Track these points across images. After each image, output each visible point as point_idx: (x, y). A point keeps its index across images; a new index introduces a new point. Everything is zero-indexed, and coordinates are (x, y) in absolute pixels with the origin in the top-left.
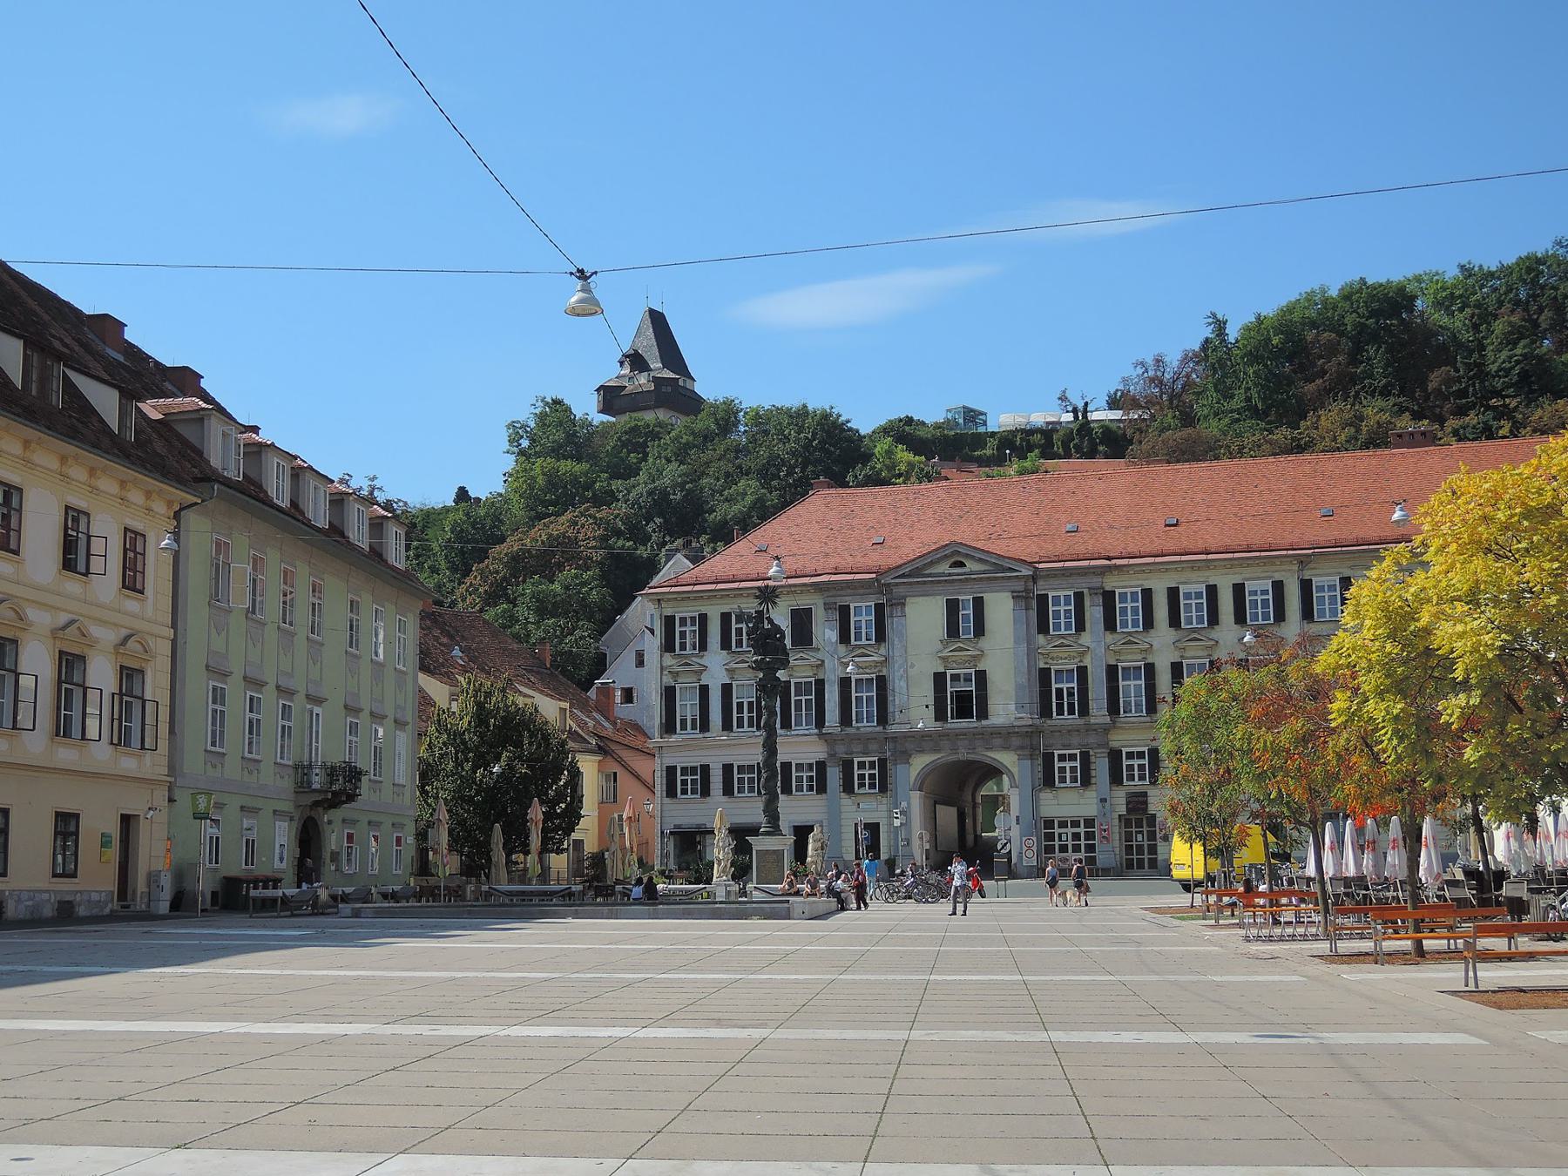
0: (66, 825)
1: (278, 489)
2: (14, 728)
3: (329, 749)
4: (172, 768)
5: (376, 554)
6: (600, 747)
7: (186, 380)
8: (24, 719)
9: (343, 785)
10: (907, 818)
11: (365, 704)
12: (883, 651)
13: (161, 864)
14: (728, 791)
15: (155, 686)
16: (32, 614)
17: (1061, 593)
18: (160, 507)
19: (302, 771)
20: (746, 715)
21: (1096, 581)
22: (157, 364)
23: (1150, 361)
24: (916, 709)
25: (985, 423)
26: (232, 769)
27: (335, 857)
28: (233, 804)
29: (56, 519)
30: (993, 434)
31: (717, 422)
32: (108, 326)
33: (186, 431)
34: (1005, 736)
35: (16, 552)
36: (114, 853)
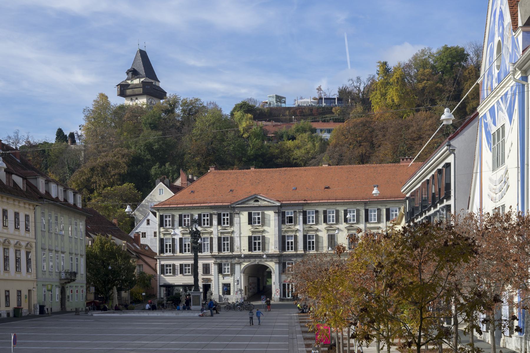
6: (137, 256)
11: (74, 252)
12: (232, 229)
13: (36, 302)
14: (181, 272)
17: (290, 211)
20: (187, 248)
21: (301, 208)
23: (355, 79)
24: (242, 246)
25: (285, 102)
27: (69, 297)
30: (289, 109)
31: (170, 105)
34: (270, 257)
36: (27, 300)
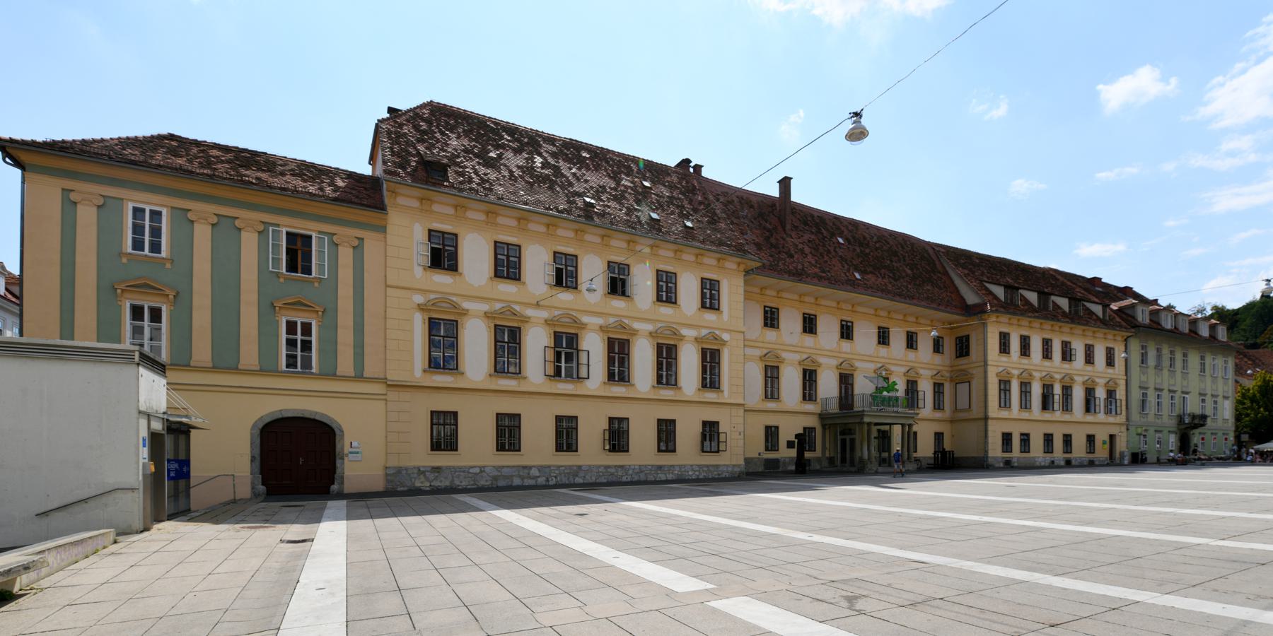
0: (1091, 439)
1: (1167, 324)
3: (1193, 407)
4: (1128, 419)
5: (1213, 337)
7: (1127, 292)
9: (1199, 421)
15: (1120, 394)
16: (1034, 374)
18: (1119, 338)
19: (1180, 419)
22: (1116, 287)
26: (1151, 418)
28: (1152, 430)
32: (1096, 281)
33: (1129, 312)
36: (1107, 446)
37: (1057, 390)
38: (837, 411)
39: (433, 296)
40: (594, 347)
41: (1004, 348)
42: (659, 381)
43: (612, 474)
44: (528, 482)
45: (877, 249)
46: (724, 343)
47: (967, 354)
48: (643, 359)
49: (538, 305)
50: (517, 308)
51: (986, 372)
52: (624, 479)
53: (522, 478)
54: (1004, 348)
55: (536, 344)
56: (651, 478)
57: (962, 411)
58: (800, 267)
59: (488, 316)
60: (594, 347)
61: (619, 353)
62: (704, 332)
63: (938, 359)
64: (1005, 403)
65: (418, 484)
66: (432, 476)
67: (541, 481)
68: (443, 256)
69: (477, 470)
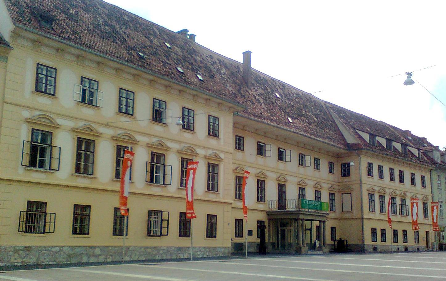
2: (50, 169)
8: (168, 181)
10: (131, 248)
29: (409, 176)
35: (193, 130)
37: (398, 202)
38: (276, 210)
39: (37, 113)
40: (64, 145)
41: (370, 173)
42: (78, 170)
43: (149, 253)
44: (93, 260)
45: (297, 102)
46: (221, 160)
47: (349, 175)
48: (104, 157)
49: (107, 125)
50: (94, 125)
51: (361, 188)
52: (157, 258)
53: (88, 256)
54: (370, 173)
55: (140, 159)
56: (174, 257)
57: (347, 212)
58: (259, 112)
59: (74, 130)
60: (64, 145)
61: (85, 150)
62: (81, 124)
63: (331, 177)
64: (372, 209)
65: (12, 260)
66: (23, 253)
67: (101, 259)
68: (45, 84)
69: (57, 249)
